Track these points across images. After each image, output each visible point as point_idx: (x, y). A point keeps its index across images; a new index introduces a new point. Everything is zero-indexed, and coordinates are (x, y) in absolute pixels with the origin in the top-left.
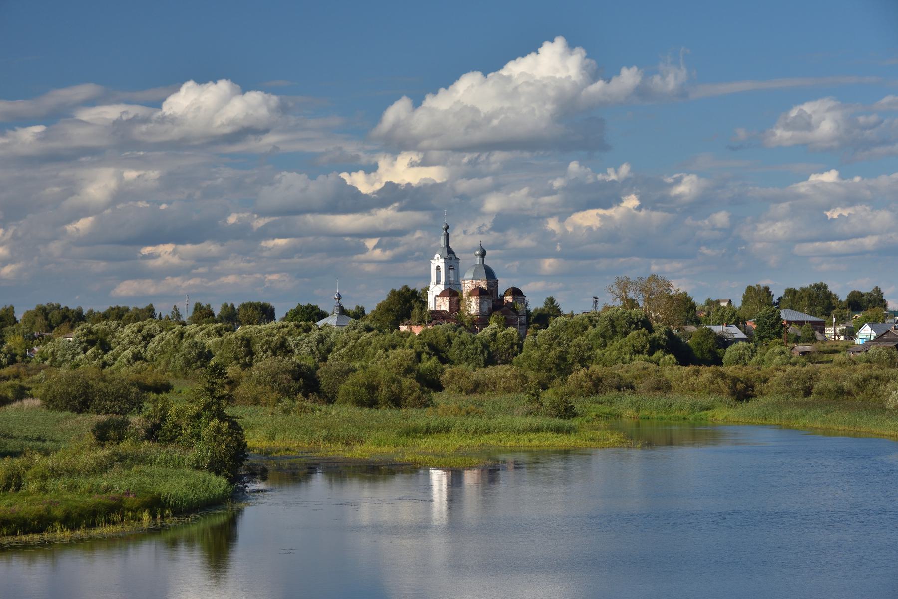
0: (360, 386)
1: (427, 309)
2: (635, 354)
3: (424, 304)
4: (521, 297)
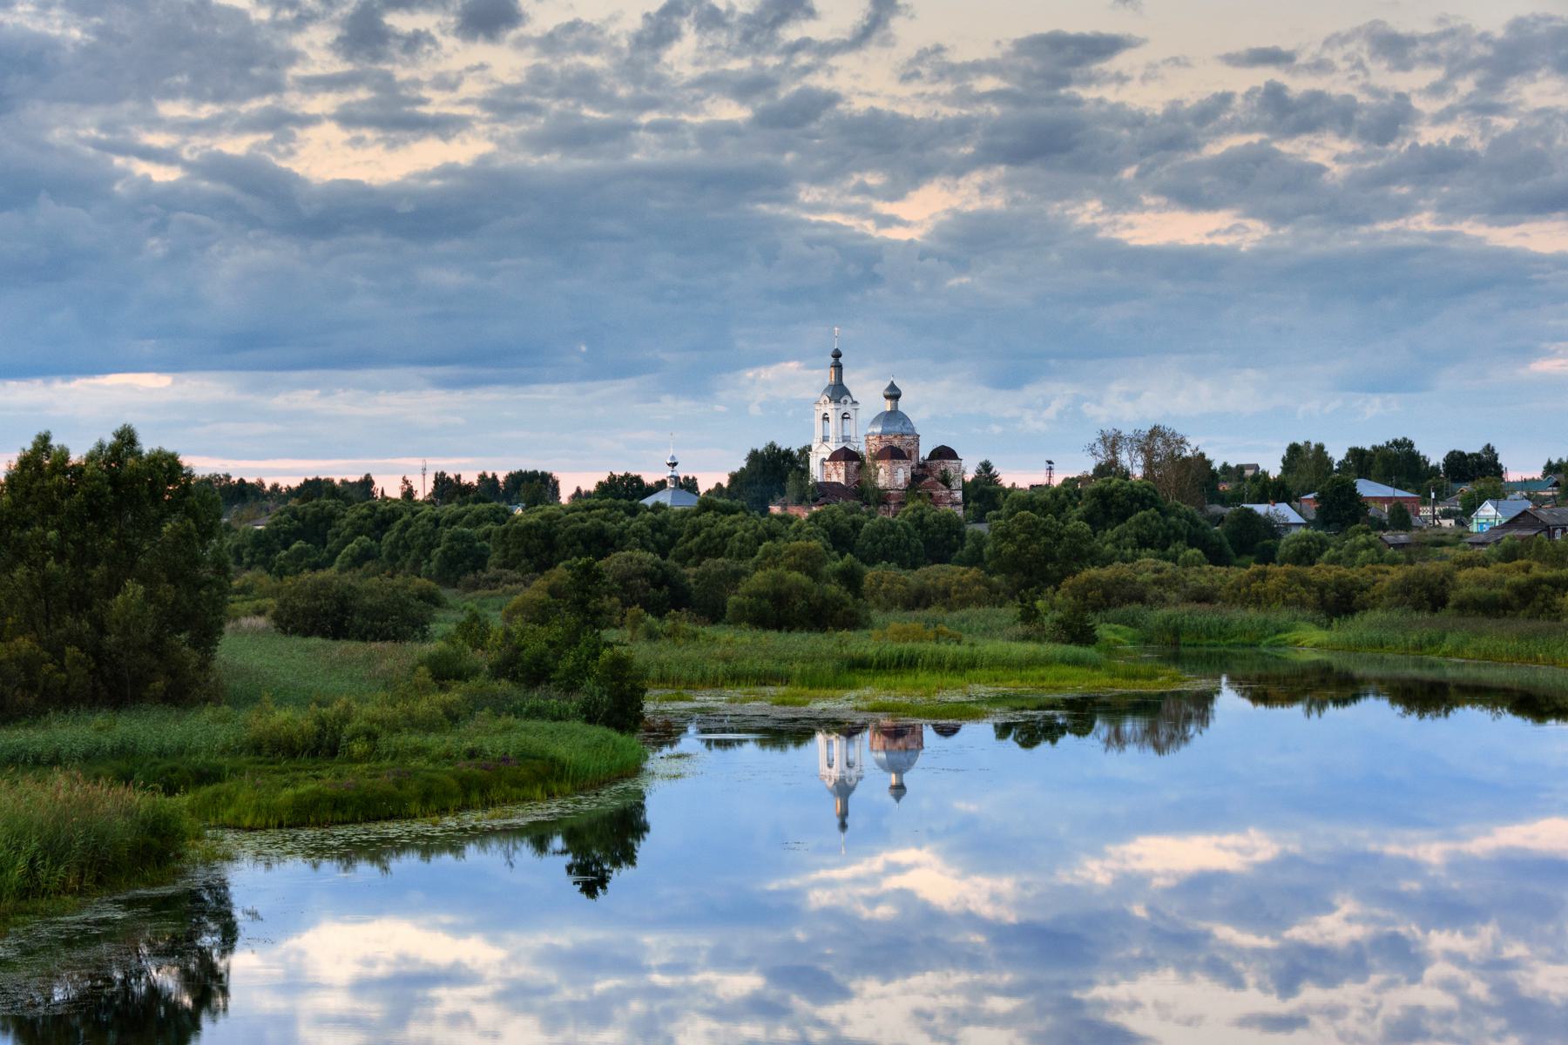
0: (760, 595)
1: (808, 479)
2: (1140, 548)
3: (805, 472)
4: (954, 461)
